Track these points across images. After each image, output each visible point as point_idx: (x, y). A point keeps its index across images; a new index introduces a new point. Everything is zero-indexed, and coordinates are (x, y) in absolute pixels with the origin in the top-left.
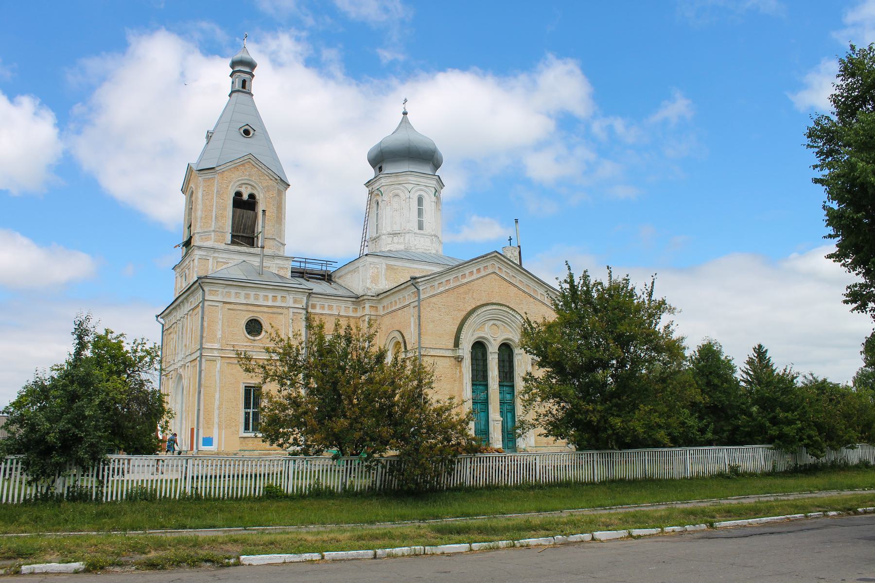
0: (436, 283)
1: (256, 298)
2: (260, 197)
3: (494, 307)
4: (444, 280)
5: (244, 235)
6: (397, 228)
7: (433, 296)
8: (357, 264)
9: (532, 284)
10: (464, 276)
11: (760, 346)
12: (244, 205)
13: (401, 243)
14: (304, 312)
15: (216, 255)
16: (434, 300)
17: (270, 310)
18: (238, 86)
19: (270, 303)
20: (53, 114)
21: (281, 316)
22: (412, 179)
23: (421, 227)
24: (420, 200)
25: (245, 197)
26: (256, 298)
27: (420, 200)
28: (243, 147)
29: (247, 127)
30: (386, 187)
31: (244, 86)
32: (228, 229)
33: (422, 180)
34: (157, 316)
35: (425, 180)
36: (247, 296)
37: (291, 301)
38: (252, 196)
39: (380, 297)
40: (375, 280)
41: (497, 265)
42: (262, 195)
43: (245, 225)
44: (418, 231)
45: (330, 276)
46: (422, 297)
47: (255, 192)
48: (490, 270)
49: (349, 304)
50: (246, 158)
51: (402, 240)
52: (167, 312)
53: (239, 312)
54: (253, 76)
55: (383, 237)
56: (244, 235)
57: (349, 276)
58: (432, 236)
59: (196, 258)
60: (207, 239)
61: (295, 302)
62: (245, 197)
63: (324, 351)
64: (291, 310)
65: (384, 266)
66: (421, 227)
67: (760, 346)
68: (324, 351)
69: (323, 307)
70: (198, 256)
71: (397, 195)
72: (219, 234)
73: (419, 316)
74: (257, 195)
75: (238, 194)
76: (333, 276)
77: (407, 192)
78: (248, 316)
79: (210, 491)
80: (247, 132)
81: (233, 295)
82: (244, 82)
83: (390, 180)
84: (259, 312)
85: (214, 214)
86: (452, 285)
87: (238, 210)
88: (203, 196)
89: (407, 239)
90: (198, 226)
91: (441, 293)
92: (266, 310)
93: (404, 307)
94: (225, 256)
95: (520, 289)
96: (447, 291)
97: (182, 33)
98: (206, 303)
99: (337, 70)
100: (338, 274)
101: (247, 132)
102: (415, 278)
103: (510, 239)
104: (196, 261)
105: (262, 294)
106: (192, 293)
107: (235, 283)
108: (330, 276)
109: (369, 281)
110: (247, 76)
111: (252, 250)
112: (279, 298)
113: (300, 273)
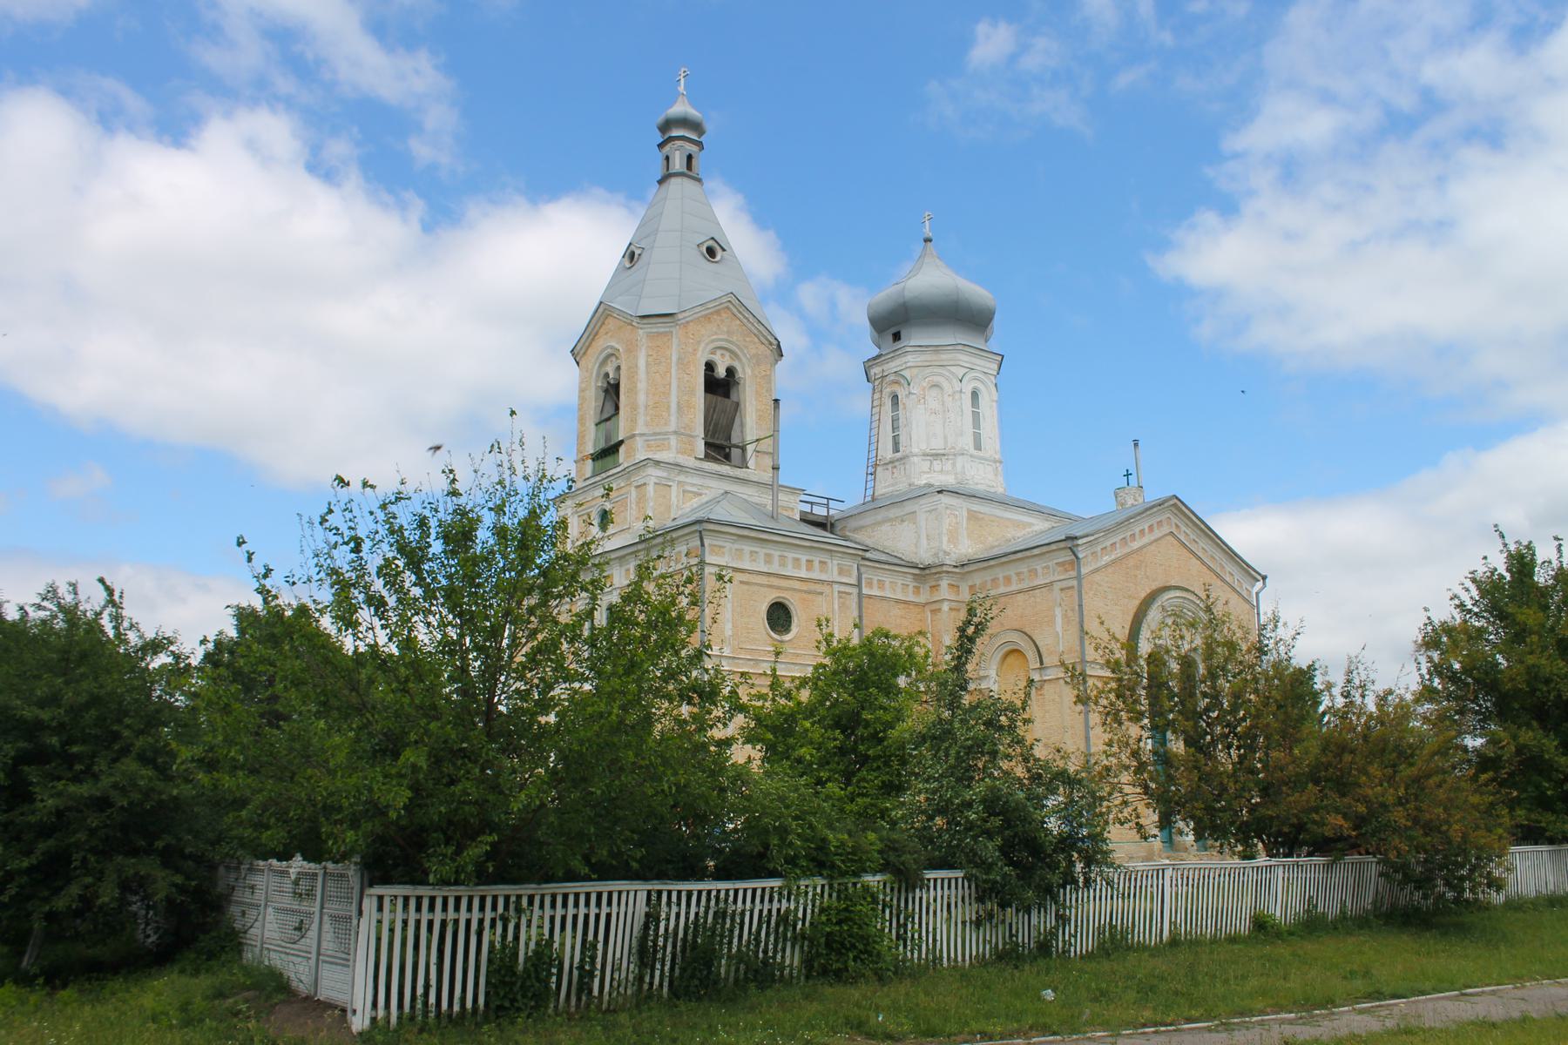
1: (783, 565)
3: (1178, 593)
4: (1108, 543)
5: (720, 446)
6: (937, 445)
7: (1097, 570)
8: (909, 507)
9: (1218, 555)
12: (720, 386)
13: (948, 473)
14: (855, 591)
15: (682, 478)
16: (1097, 577)
17: (804, 587)
18: (678, 164)
19: (803, 574)
21: (820, 598)
22: (964, 358)
23: (978, 447)
24: (975, 395)
25: (721, 372)
26: (783, 565)
27: (975, 395)
29: (711, 243)
30: (915, 371)
33: (978, 361)
36: (768, 559)
37: (835, 569)
38: (730, 371)
39: (966, 569)
40: (953, 539)
41: (1174, 520)
42: (749, 371)
43: (716, 425)
44: (975, 453)
45: (832, 525)
46: (1084, 571)
47: (737, 365)
48: (1166, 529)
49: (909, 580)
51: (948, 466)
53: (756, 588)
57: (886, 528)
58: (995, 461)
61: (841, 572)
62: (721, 372)
64: (836, 587)
65: (965, 514)
66: (978, 447)
69: (881, 584)
70: (654, 480)
71: (936, 386)
73: (1080, 606)
74: (739, 369)
75: (710, 367)
77: (955, 382)
78: (772, 597)
80: (711, 252)
81: (747, 556)
82: (690, 157)
83: (923, 357)
84: (787, 589)
86: (1119, 552)
88: (648, 364)
89: (959, 465)
90: (641, 420)
91: (1106, 566)
92: (797, 585)
93: (1034, 589)
94: (696, 480)
95: (1203, 563)
96: (1114, 562)
97: (65, 92)
99: (353, 181)
101: (711, 252)
103: (1128, 475)
104: (650, 488)
105: (791, 555)
107: (753, 534)
108: (832, 525)
109: (945, 539)
110: (693, 149)
111: (725, 469)
112: (816, 564)
113: (807, 520)
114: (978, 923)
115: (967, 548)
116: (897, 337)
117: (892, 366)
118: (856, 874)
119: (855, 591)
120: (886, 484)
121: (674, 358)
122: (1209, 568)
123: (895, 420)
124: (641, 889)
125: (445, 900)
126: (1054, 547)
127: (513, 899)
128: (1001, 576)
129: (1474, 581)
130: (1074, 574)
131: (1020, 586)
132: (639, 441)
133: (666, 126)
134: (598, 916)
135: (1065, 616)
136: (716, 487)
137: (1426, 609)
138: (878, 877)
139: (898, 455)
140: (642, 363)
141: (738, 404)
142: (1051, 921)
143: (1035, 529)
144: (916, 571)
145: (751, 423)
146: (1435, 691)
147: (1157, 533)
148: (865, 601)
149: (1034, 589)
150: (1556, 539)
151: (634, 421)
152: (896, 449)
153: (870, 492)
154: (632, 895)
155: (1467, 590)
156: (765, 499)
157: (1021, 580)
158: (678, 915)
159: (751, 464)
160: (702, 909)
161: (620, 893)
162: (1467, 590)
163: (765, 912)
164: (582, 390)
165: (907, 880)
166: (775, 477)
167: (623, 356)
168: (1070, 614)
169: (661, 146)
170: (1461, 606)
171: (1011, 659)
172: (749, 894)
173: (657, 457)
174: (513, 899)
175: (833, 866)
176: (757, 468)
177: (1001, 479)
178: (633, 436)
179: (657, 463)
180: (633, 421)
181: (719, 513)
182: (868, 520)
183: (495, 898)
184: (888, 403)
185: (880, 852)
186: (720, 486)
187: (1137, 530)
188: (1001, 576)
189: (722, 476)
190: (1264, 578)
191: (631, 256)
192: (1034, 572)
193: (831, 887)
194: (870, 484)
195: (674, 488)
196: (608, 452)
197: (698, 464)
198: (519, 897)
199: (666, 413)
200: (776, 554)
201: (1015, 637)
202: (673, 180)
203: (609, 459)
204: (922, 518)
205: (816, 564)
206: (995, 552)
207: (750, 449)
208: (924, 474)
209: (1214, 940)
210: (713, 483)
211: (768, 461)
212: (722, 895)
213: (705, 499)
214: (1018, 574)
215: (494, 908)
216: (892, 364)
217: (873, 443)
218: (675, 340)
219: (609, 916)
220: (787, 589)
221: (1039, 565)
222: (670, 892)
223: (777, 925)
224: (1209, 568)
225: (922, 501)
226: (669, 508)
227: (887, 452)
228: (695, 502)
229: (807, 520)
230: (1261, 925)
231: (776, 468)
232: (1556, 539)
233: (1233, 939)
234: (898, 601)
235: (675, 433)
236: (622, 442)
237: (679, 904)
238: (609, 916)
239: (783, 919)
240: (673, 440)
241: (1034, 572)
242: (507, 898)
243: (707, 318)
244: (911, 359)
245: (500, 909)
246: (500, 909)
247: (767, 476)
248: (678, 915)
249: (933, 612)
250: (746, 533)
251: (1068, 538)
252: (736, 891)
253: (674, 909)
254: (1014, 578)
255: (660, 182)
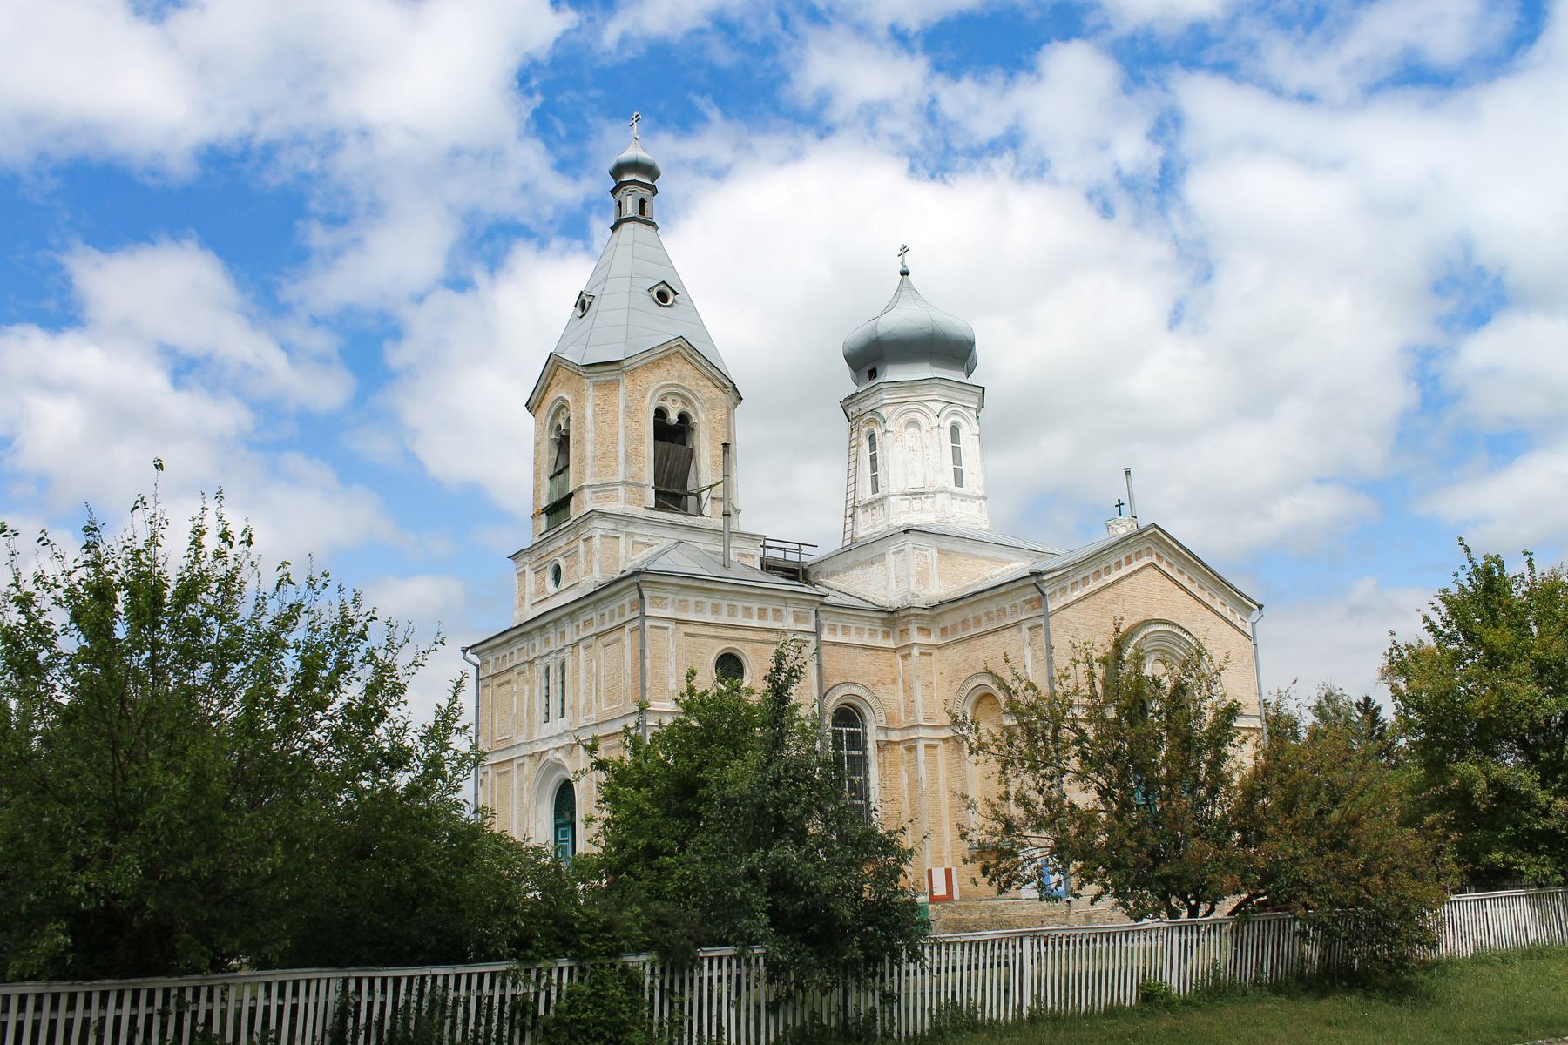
0: (1069, 583)
2: (700, 419)
3: (1161, 627)
5: (673, 492)
6: (916, 483)
10: (1108, 570)
11: (1368, 700)
12: (672, 434)
15: (631, 529)
16: (1067, 613)
18: (630, 209)
19: (755, 623)
20: (191, 246)
22: (938, 393)
23: (959, 481)
24: (955, 430)
25: (673, 418)
27: (955, 430)
28: (660, 327)
29: (662, 287)
30: (891, 408)
31: (642, 212)
32: (649, 478)
33: (957, 395)
34: (464, 651)
35: (962, 396)
39: (937, 611)
40: (923, 579)
42: (702, 416)
43: (670, 473)
45: (805, 571)
46: (1051, 607)
47: (688, 409)
48: (1145, 561)
49: (877, 625)
50: (674, 344)
52: (498, 641)
54: (655, 192)
55: (892, 499)
56: (673, 492)
57: (857, 572)
58: (979, 498)
59: (598, 533)
60: (609, 499)
61: (797, 619)
62: (673, 418)
63: (1132, 701)
66: (959, 481)
67: (1368, 700)
68: (1132, 701)
70: (600, 532)
72: (634, 489)
75: (660, 414)
76: (812, 571)
79: (954, 994)
80: (662, 297)
82: (642, 202)
84: (738, 640)
85: (621, 449)
87: (661, 443)
88: (595, 415)
90: (589, 471)
92: (749, 635)
93: (1003, 629)
94: (646, 531)
96: (1086, 597)
98: (648, 623)
100: (825, 568)
101: (662, 297)
102: (1041, 574)
103: (1120, 505)
104: (596, 541)
106: (595, 603)
107: (697, 584)
108: (805, 571)
109: (913, 580)
110: (645, 193)
111: (677, 518)
112: (769, 612)
113: (769, 567)
114: (773, 1008)
115: (938, 588)
116: (873, 374)
117: (869, 404)
118: (617, 956)
119: (813, 639)
120: (866, 526)
121: (621, 407)
122: (1197, 599)
123: (873, 459)
124: (335, 975)
125: (89, 996)
126: (1019, 584)
127: (174, 992)
128: (970, 617)
129: (1443, 599)
130: (1040, 611)
131: (990, 627)
132: (587, 493)
133: (618, 170)
134: (280, 1009)
135: (1034, 656)
136: (666, 538)
137: (1392, 634)
138: (643, 958)
139: (877, 496)
140: (589, 413)
141: (692, 451)
142: (875, 1000)
143: (1018, 567)
144: (885, 616)
145: (705, 469)
146: (1411, 723)
147: (1136, 565)
148: (824, 649)
149: (1003, 629)
150: (1526, 553)
151: (582, 472)
152: (875, 490)
153: (848, 535)
154: (323, 984)
155: (1437, 609)
156: (714, 546)
157: (990, 620)
158: (383, 1005)
159: (707, 510)
160: (414, 998)
161: (308, 982)
162: (1437, 609)
163: (201, 1019)
164: (537, 444)
165: (678, 962)
166: (727, 525)
167: (571, 406)
168: (1039, 653)
169: (614, 192)
170: (1432, 628)
171: (985, 701)
172: (475, 980)
173: (606, 508)
174: (174, 992)
175: (577, 946)
176: (712, 515)
177: (985, 515)
178: (581, 488)
179: (603, 515)
180: (584, 472)
181: (663, 565)
182: (839, 564)
183: (151, 993)
184: (866, 443)
185: (645, 928)
186: (672, 536)
187: (1112, 562)
188: (970, 617)
189: (673, 525)
190: (1260, 607)
191: (583, 304)
192: (1002, 611)
193: (582, 970)
194: (849, 527)
195: (623, 537)
196: (558, 508)
197: (649, 514)
198: (182, 990)
199: (617, 458)
200: (724, 603)
201: (986, 681)
202: (625, 226)
203: (562, 513)
204: (890, 558)
205: (769, 612)
206: (971, 591)
207: (704, 495)
208: (901, 514)
209: (1088, 1015)
210: (667, 533)
211: (720, 508)
212: (440, 982)
213: (656, 549)
214: (987, 614)
215: (150, 1002)
216: (868, 403)
217: (852, 485)
218: (622, 388)
219: (294, 1008)
220: (738, 640)
221: (1007, 604)
222: (372, 980)
223: (513, 1013)
224: (1197, 599)
225: (890, 542)
226: (617, 561)
227: (866, 494)
228: (646, 553)
229: (769, 567)
230: (1151, 997)
231: (726, 515)
232: (1526, 553)
233: (1112, 1012)
234: (865, 647)
235: (624, 483)
236: (571, 495)
237: (384, 992)
238: (294, 1008)
239: (522, 1007)
240: (621, 490)
241: (1002, 611)
242: (167, 991)
243: (657, 364)
244: (887, 397)
245: (158, 1004)
246: (158, 1004)
247: (718, 522)
248: (383, 1005)
249: (904, 657)
250: (689, 583)
251: (1033, 574)
252: (458, 977)
253: (378, 998)
254: (984, 619)
255: (614, 228)
